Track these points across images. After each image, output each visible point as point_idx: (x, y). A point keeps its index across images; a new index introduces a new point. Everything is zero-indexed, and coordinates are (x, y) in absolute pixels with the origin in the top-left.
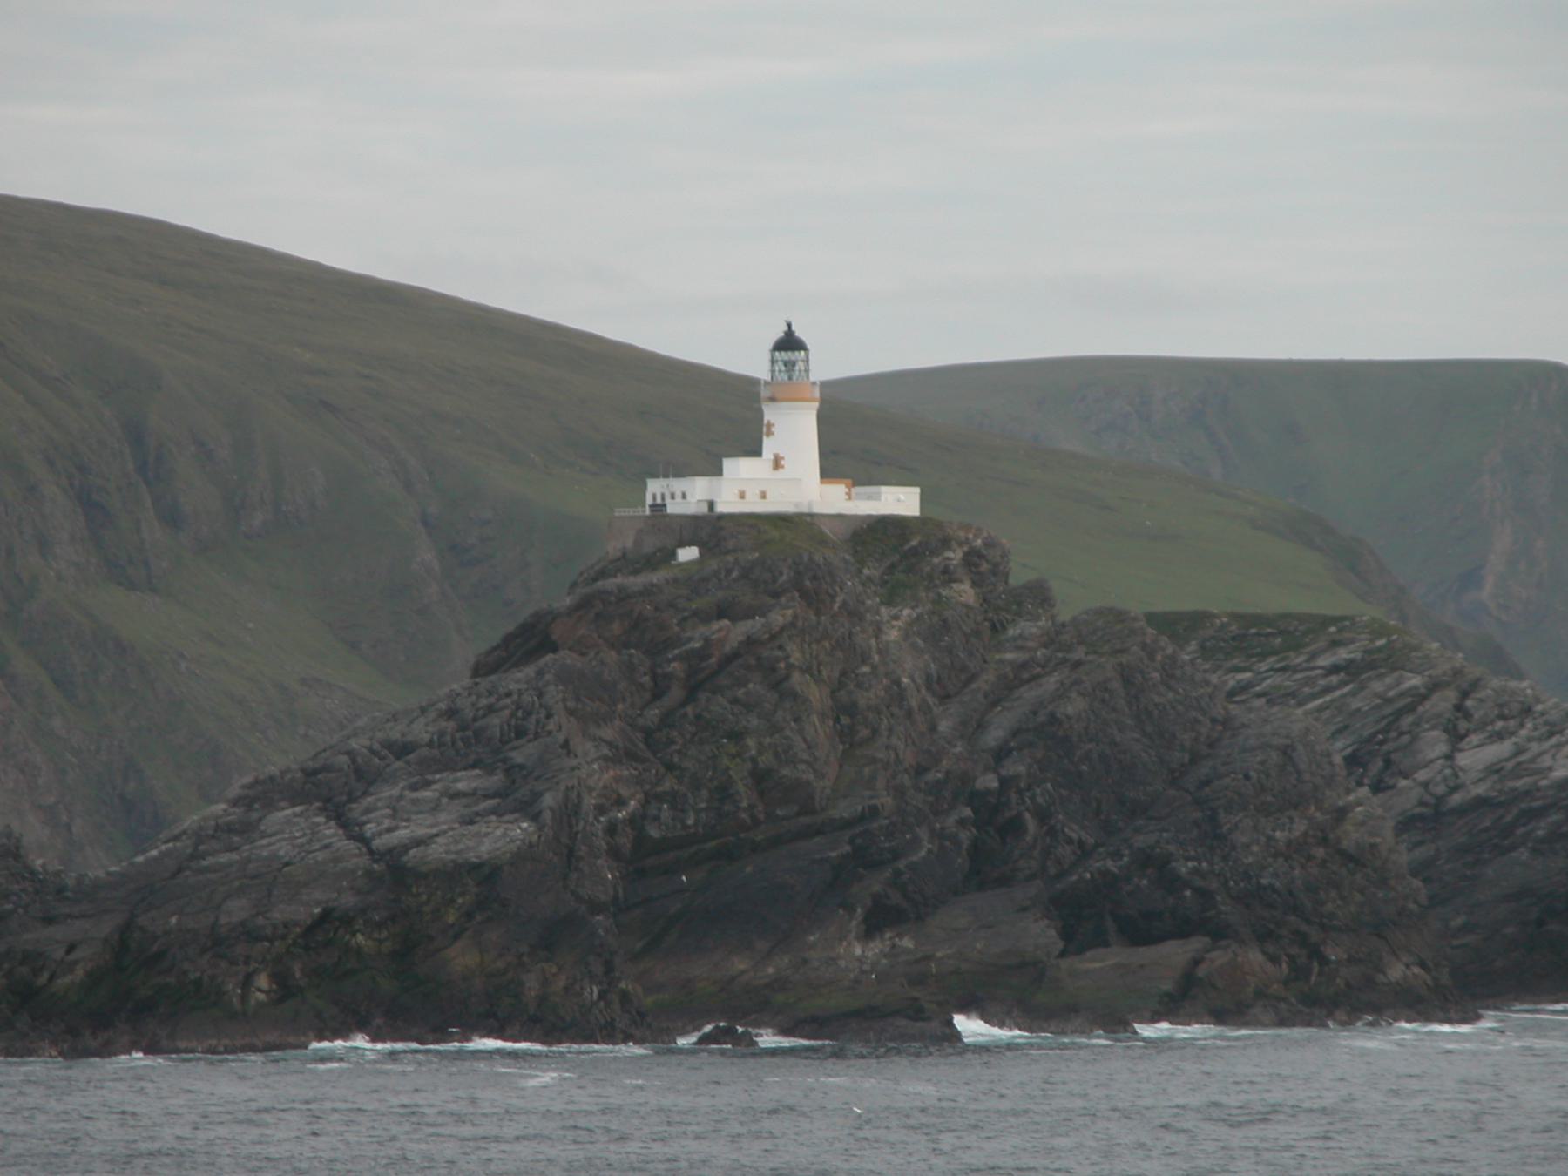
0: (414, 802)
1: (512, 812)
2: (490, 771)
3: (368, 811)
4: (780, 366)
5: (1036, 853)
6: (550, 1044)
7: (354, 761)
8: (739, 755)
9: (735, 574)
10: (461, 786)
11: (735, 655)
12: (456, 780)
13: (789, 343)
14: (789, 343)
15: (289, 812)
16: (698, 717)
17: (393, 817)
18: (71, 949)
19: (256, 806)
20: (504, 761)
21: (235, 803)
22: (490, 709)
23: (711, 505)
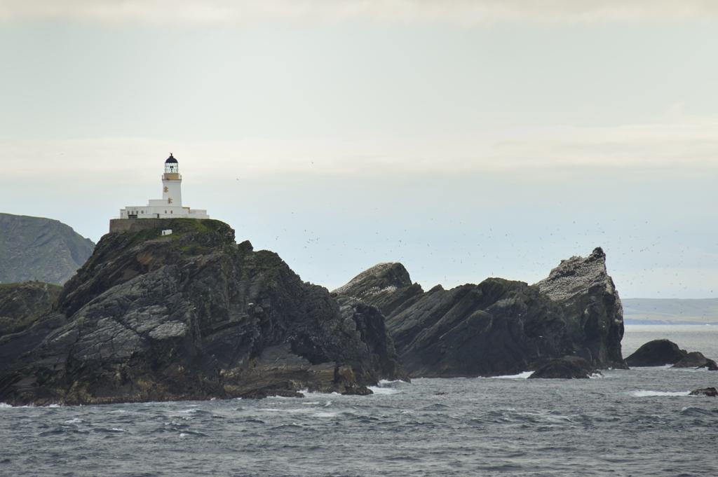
0: (142, 316)
1: (175, 320)
2: (162, 306)
3: (129, 319)
4: (169, 168)
5: (273, 334)
6: (392, 380)
7: (119, 302)
8: (206, 300)
9: (193, 239)
10: (155, 310)
11: (205, 266)
12: (152, 309)
13: (171, 160)
14: (171, 160)
15: (104, 319)
16: (195, 287)
17: (137, 321)
18: (55, 366)
19: (93, 317)
20: (166, 302)
21: (86, 316)
22: (156, 285)
23: (158, 215)
